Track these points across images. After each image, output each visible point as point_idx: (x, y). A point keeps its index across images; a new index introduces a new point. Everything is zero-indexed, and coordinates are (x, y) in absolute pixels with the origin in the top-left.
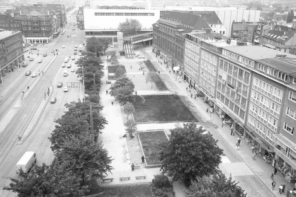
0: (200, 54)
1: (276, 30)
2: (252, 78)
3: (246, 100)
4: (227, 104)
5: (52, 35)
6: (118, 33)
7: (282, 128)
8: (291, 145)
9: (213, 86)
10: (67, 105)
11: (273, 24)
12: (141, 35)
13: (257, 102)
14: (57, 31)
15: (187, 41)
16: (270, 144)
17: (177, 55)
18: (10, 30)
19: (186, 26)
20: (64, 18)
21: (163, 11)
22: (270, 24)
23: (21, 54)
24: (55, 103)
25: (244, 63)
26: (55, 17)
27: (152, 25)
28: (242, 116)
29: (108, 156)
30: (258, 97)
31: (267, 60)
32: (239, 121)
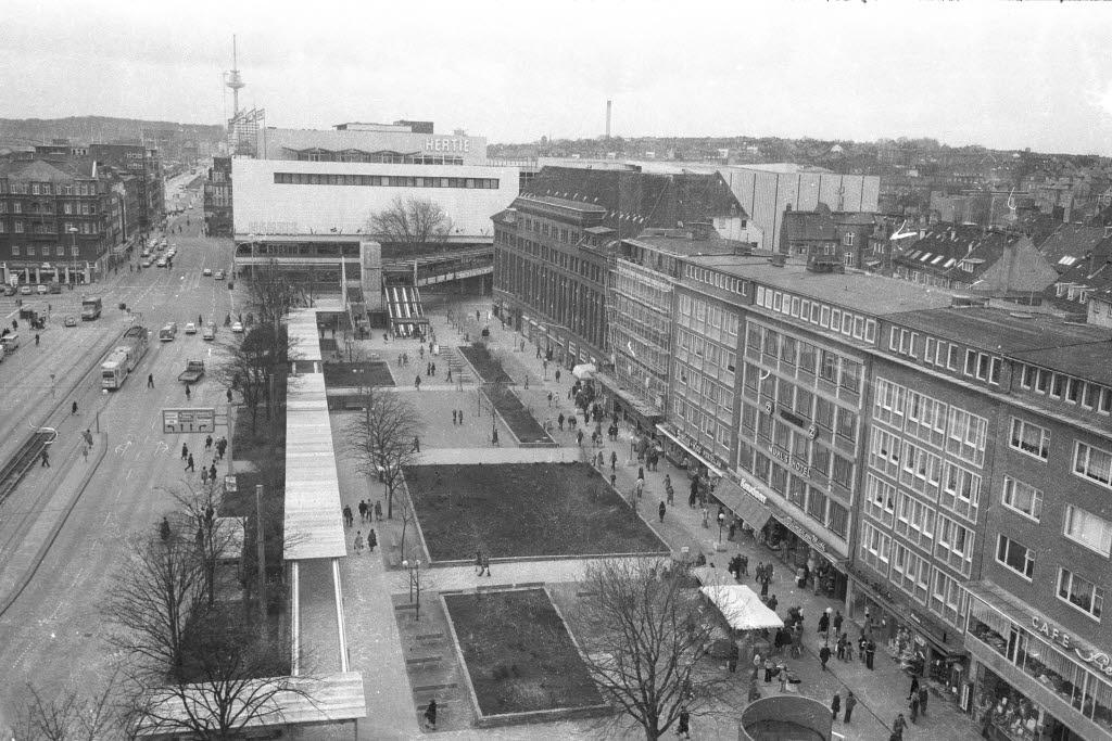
1: (940, 239)
2: (867, 405)
3: (851, 465)
4: (779, 488)
7: (991, 557)
8: (1026, 617)
9: (725, 425)
11: (927, 221)
13: (892, 469)
14: (124, 242)
19: (617, 216)
25: (837, 330)
27: (492, 218)
28: (836, 529)
30: (895, 450)
32: (829, 549)
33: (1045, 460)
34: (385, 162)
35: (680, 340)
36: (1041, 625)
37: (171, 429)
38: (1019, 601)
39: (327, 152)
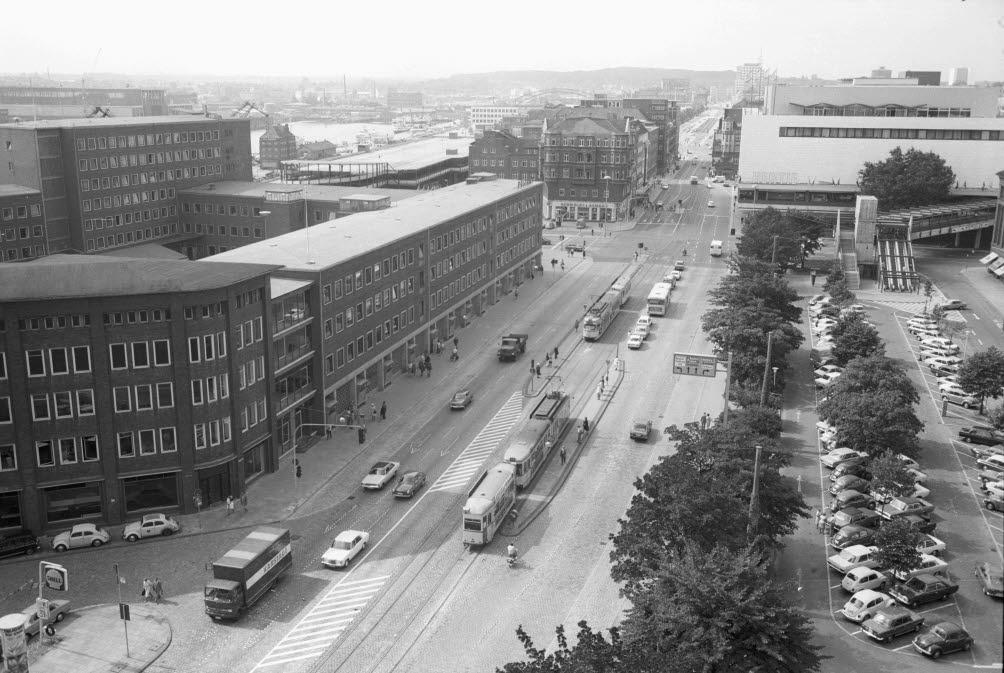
5: (630, 198)
12: (947, 209)
14: (644, 184)
18: (509, 177)
20: (671, 144)
23: (535, 250)
24: (463, 412)
26: (644, 138)
34: (816, 115)
37: (679, 371)
39: (831, 107)
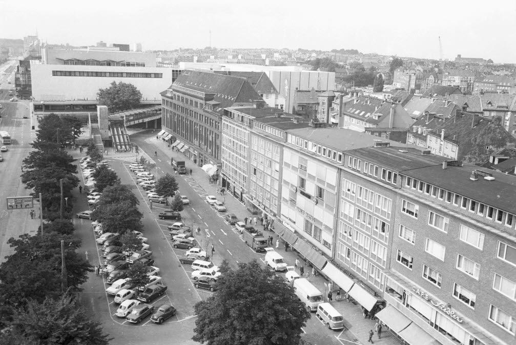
0: (250, 143)
6: (98, 107)
10: (12, 241)
15: (225, 120)
16: (364, 278)
17: (189, 134)
19: (221, 96)
21: (177, 71)
22: (353, 95)
29: (103, 335)
31: (362, 151)
33: (417, 218)
35: (253, 156)
36: (416, 290)
38: (406, 278)
